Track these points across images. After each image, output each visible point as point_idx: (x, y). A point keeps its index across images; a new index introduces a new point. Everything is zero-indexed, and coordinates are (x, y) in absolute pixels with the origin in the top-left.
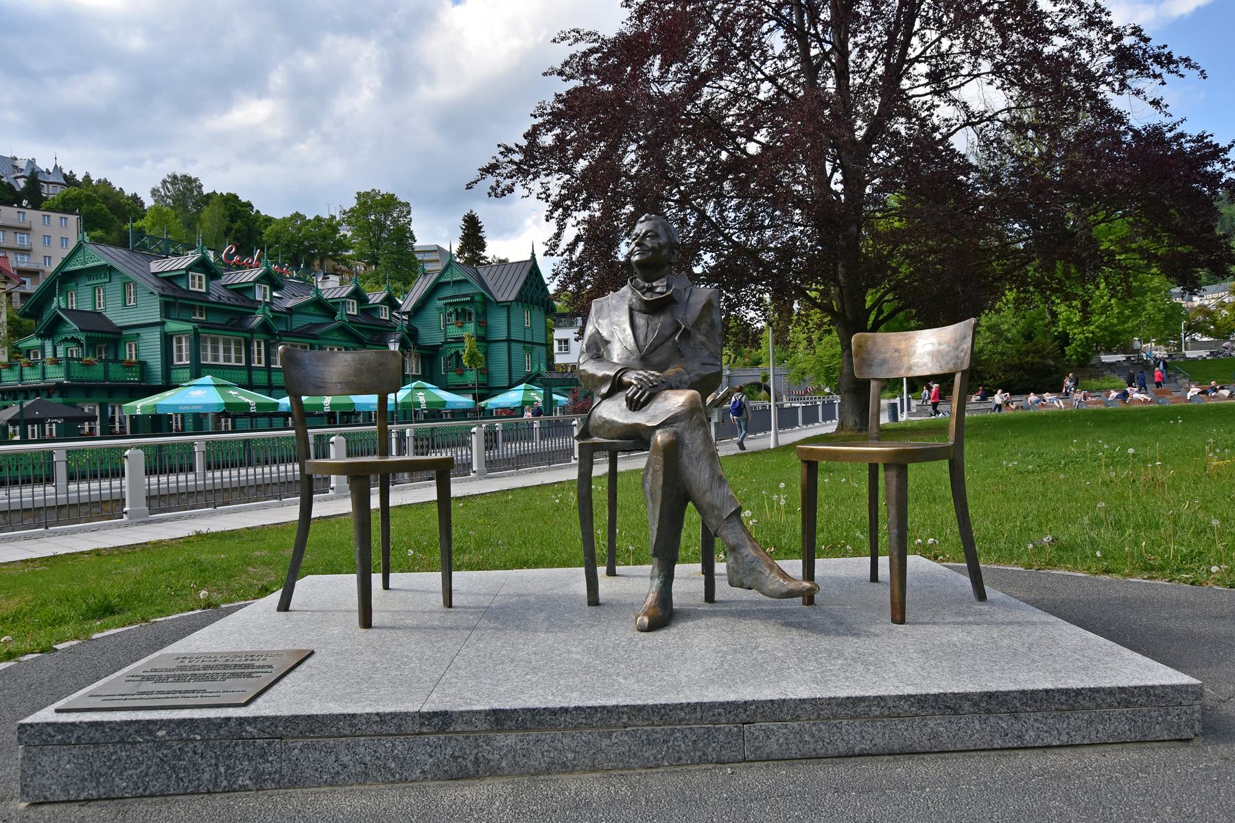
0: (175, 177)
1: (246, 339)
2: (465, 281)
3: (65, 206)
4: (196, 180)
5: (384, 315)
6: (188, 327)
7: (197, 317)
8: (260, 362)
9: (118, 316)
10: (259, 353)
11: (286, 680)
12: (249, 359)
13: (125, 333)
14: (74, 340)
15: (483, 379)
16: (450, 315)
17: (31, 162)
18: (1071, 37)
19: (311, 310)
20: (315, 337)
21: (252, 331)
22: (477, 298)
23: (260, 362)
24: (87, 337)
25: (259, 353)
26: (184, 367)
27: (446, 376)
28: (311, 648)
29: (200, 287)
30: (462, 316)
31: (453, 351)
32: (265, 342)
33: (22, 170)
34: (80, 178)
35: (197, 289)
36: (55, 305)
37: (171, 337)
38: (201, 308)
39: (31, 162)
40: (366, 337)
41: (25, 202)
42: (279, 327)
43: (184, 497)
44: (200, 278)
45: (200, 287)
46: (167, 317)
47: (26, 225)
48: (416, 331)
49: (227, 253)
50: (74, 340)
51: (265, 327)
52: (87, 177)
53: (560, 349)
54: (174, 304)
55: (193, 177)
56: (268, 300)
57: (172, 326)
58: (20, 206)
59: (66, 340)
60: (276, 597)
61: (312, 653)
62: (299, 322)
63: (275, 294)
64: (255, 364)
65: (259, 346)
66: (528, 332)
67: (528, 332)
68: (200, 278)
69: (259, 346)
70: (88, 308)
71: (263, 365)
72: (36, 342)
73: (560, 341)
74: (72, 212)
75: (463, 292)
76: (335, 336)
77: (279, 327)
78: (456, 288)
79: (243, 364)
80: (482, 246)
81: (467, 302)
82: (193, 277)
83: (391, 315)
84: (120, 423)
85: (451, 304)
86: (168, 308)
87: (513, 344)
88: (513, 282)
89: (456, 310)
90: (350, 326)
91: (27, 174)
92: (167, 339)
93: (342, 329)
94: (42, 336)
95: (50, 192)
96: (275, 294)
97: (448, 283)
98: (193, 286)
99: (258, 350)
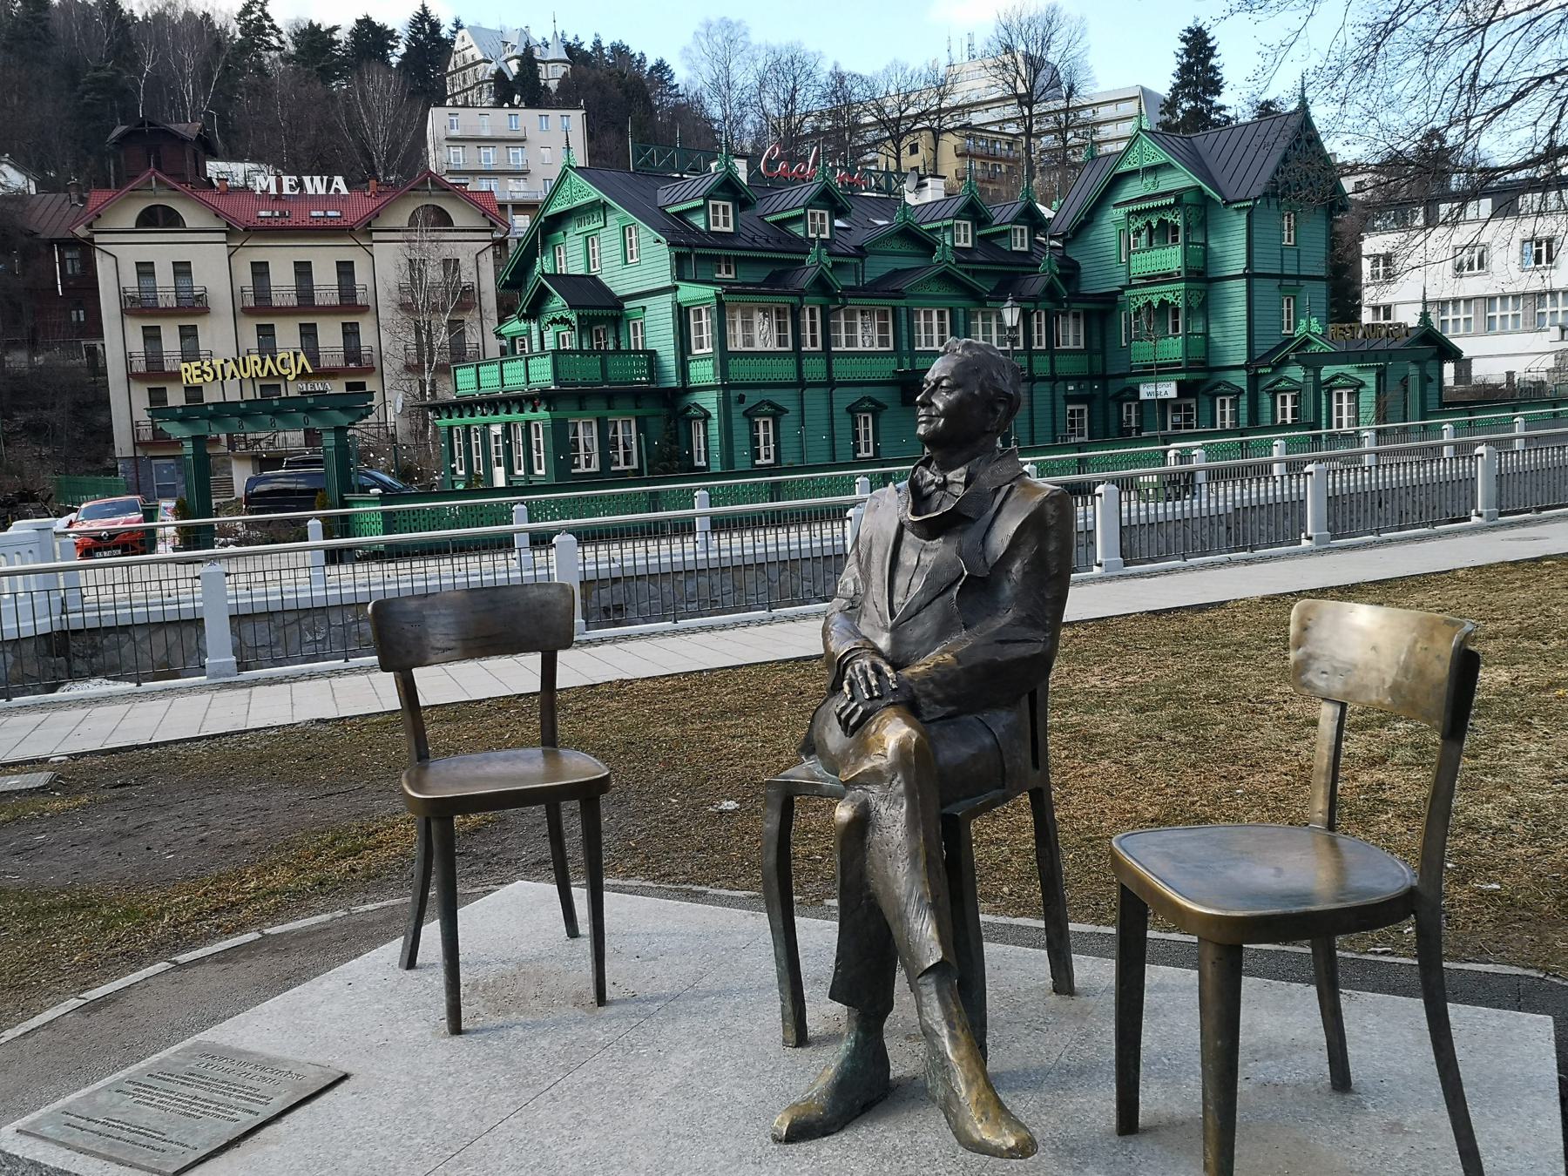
0: (709, 26)
1: (792, 305)
2: (1167, 166)
3: (566, 98)
4: (739, 24)
5: (1020, 243)
6: (708, 292)
7: (723, 275)
8: (814, 344)
9: (620, 281)
10: (813, 329)
11: (298, 1112)
12: (798, 341)
13: (627, 305)
14: (564, 321)
15: (1197, 354)
16: (1138, 233)
17: (524, 32)
18: (175, 962)
19: (896, 246)
20: (898, 294)
21: (801, 294)
22: (1187, 198)
23: (814, 344)
24: (579, 317)
25: (813, 326)
26: (703, 358)
27: (1129, 347)
28: (346, 1069)
29: (726, 224)
30: (1162, 233)
31: (1141, 302)
32: (822, 308)
33: (514, 47)
34: (587, 47)
35: (721, 228)
36: (538, 269)
37: (688, 308)
38: (728, 258)
39: (524, 32)
40: (986, 286)
41: (517, 98)
42: (843, 281)
43: (681, 578)
44: (725, 209)
45: (726, 224)
46: (680, 279)
47: (520, 135)
48: (1075, 266)
49: (768, 160)
50: (564, 321)
51: (822, 285)
52: (597, 45)
53: (1375, 275)
54: (688, 256)
55: (735, 20)
56: (826, 236)
57: (688, 292)
58: (512, 106)
59: (554, 321)
60: (395, 947)
61: (345, 1077)
62: (876, 268)
63: (838, 223)
64: (808, 348)
65: (813, 316)
66: (1290, 257)
67: (1290, 257)
68: (725, 209)
69: (813, 316)
70: (580, 270)
71: (819, 347)
72: (523, 325)
73: (1376, 258)
74: (576, 107)
75: (1161, 189)
76: (934, 289)
77: (843, 281)
78: (1150, 180)
79: (790, 348)
80: (1215, 87)
81: (1169, 207)
82: (715, 207)
83: (1032, 241)
84: (625, 447)
85: (1139, 213)
86: (683, 266)
87: (1257, 282)
88: (1243, 168)
89: (1149, 224)
90: (958, 271)
91: (519, 51)
92: (682, 314)
93: (945, 277)
94: (525, 318)
95: (551, 76)
96: (838, 223)
97: (1133, 173)
98: (716, 224)
99: (810, 322)
